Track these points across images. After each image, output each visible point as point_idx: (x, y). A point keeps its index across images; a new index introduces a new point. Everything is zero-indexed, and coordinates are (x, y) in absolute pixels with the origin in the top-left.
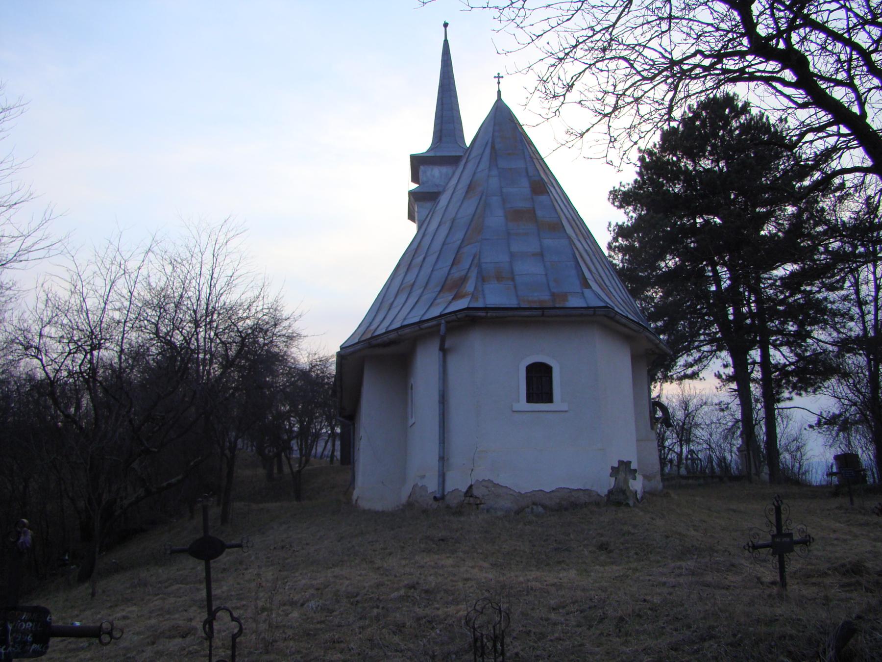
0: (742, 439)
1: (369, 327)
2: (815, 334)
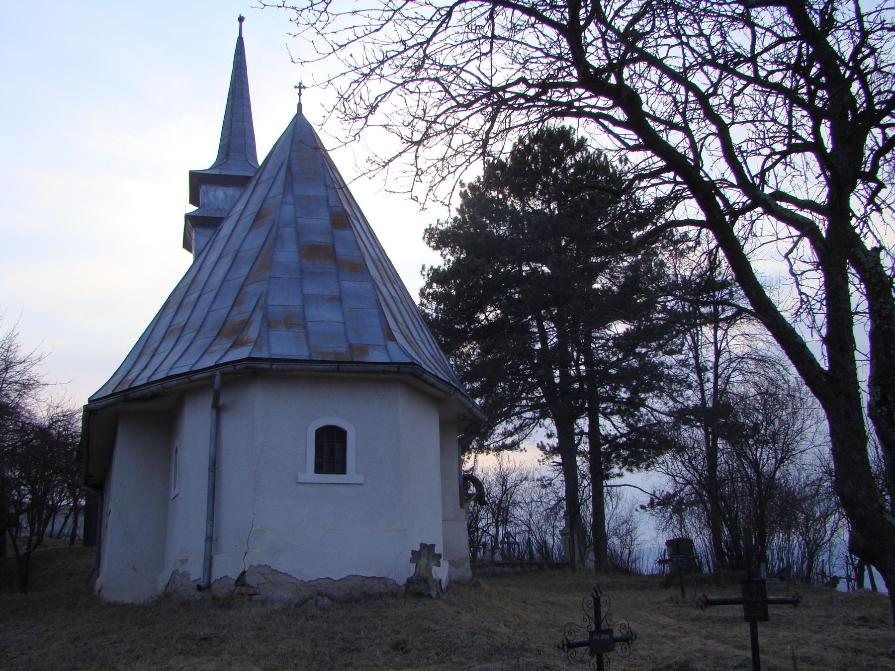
0: (566, 520)
1: (126, 376)
2: (649, 402)
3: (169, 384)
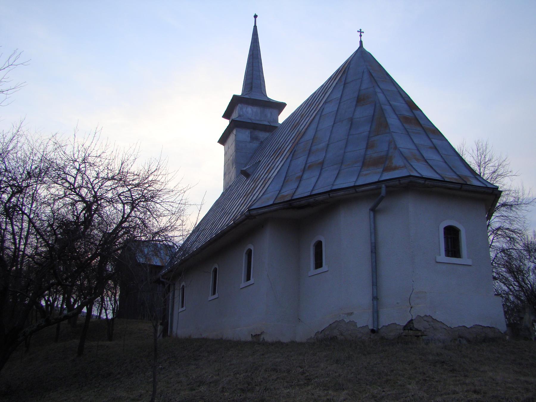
3: (335, 195)
